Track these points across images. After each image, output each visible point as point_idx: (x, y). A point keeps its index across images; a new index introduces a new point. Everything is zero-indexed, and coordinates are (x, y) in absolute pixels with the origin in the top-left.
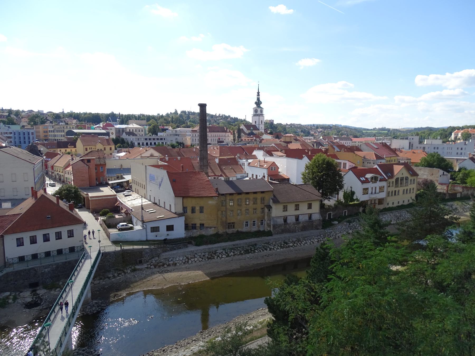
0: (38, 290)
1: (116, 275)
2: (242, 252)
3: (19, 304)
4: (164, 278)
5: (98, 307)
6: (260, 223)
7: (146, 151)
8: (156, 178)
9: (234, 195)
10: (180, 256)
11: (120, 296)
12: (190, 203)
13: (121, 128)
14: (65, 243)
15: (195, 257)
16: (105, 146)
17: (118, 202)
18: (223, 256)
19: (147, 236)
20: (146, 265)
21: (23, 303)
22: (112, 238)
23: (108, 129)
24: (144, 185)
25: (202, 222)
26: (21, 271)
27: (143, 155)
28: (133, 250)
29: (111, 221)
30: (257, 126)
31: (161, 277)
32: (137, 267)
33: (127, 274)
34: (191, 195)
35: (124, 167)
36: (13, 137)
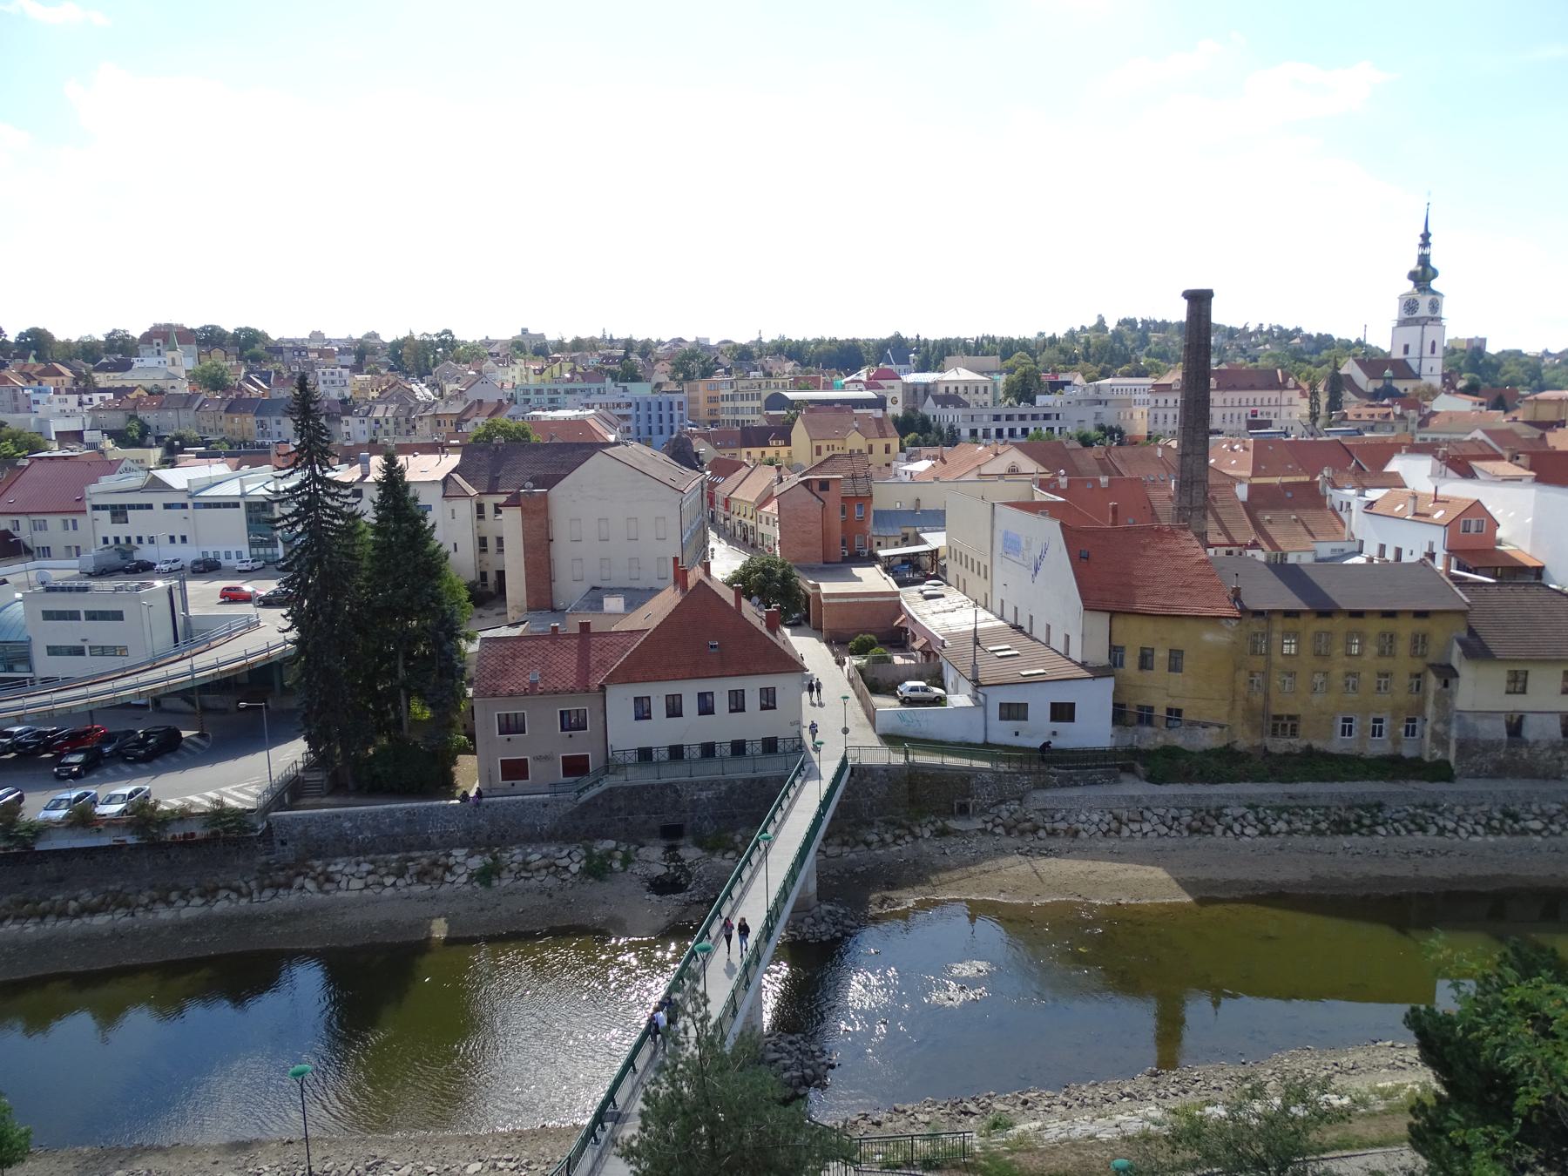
0: (680, 847)
1: (888, 837)
3: (634, 878)
4: (1035, 872)
5: (834, 924)
6: (1402, 730)
7: (997, 455)
8: (1023, 545)
9: (1303, 618)
10: (1090, 810)
11: (899, 904)
12: (1136, 635)
13: (920, 384)
14: (753, 725)
15: (1144, 820)
17: (903, 616)
19: (986, 729)
20: (980, 820)
23: (881, 387)
24: (986, 567)
25: (1176, 704)
26: (645, 787)
27: (984, 470)
28: (942, 769)
29: (881, 673)
30: (1414, 364)
32: (953, 824)
34: (1138, 607)
35: (925, 506)
36: (634, 417)
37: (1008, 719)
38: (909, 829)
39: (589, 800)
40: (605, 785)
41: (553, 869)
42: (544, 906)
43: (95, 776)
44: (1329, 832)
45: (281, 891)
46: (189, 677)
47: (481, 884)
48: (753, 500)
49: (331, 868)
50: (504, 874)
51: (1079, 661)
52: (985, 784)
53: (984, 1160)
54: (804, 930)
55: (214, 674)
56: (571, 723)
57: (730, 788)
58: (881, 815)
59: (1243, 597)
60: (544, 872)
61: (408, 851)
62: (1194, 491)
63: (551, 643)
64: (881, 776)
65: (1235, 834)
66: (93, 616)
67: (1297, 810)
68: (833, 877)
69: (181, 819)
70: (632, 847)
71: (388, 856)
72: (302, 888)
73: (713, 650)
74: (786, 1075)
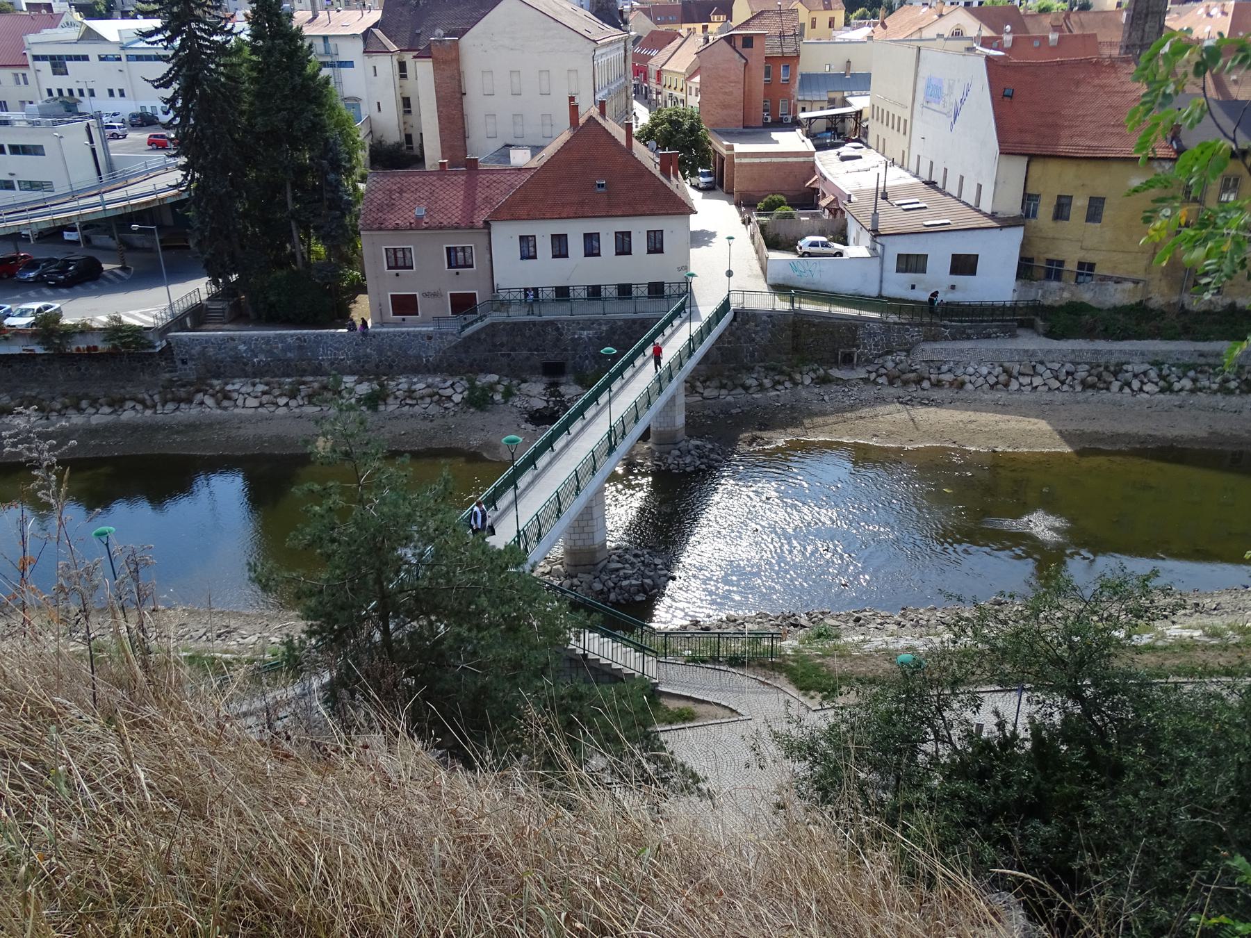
0: (562, 384)
1: (767, 383)
2: (1233, 385)
3: (514, 410)
4: (913, 420)
5: (700, 457)
7: (941, 16)
8: (945, 90)
10: (980, 363)
11: (768, 443)
16: (814, 14)
17: (816, 177)
18: (1146, 388)
20: (864, 370)
21: (525, 408)
22: (779, 276)
24: (905, 121)
25: (1089, 257)
28: (829, 317)
29: (784, 229)
31: (905, 415)
32: (835, 373)
33: (800, 387)
34: (1063, 149)
35: (855, 69)
37: (906, 271)
38: (789, 375)
39: (473, 334)
40: (487, 321)
41: (437, 397)
42: (425, 430)
43: (18, 297)
44: (1238, 391)
45: (183, 405)
46: (100, 208)
47: (369, 408)
48: (684, 71)
49: (229, 387)
50: (390, 400)
51: (989, 212)
52: (872, 335)
53: (793, 661)
54: (670, 461)
55: (125, 207)
56: (456, 259)
57: (611, 328)
58: (762, 361)
59: (1182, 135)
60: (428, 400)
61: (302, 376)
62: (1147, 26)
63: (438, 179)
64: (765, 322)
65: (1133, 391)
66: (15, 150)
67: (1206, 368)
68: (708, 417)
69: (82, 332)
70: (515, 382)
71: (282, 379)
72: (202, 403)
73: (600, 190)
74: (625, 583)
